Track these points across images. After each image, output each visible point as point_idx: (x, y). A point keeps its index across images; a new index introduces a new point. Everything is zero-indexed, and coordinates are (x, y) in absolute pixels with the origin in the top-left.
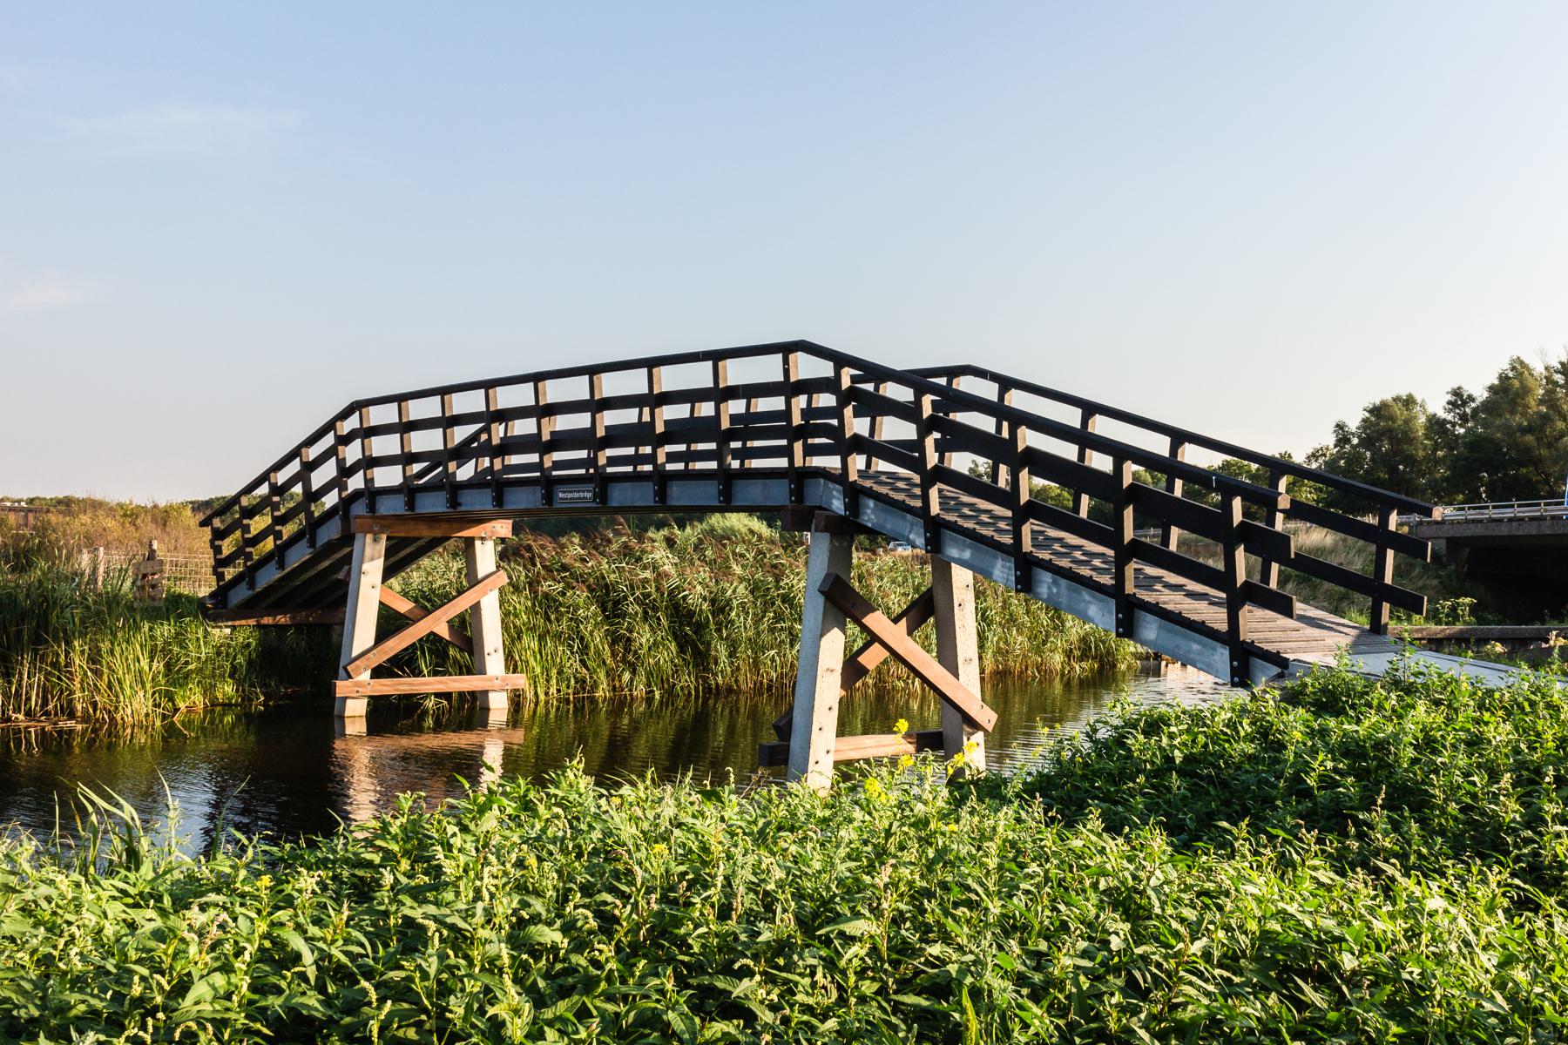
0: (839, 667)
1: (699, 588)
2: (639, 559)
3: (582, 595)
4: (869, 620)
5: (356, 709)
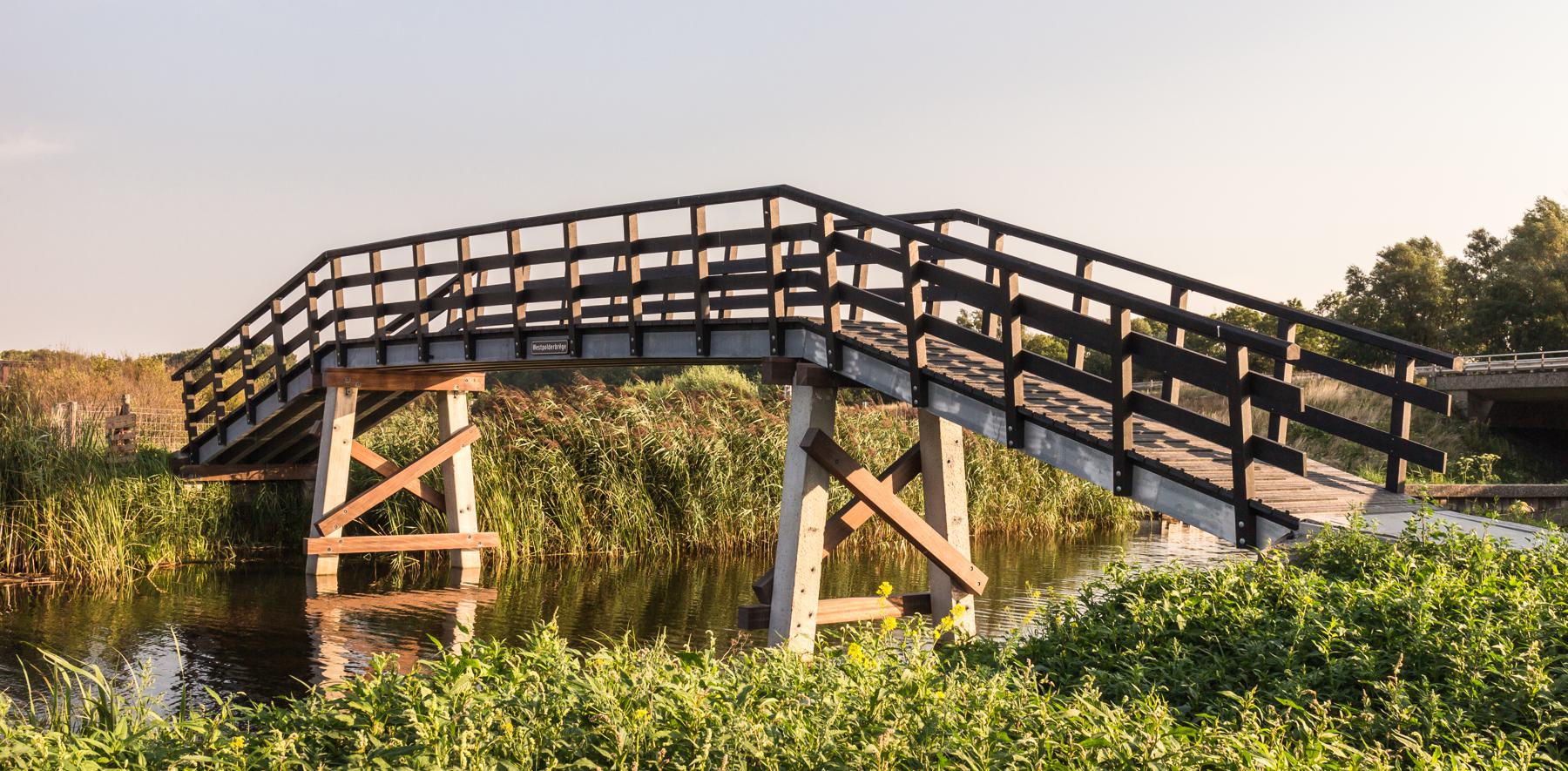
3: (552, 452)
4: (853, 478)
5: (328, 567)
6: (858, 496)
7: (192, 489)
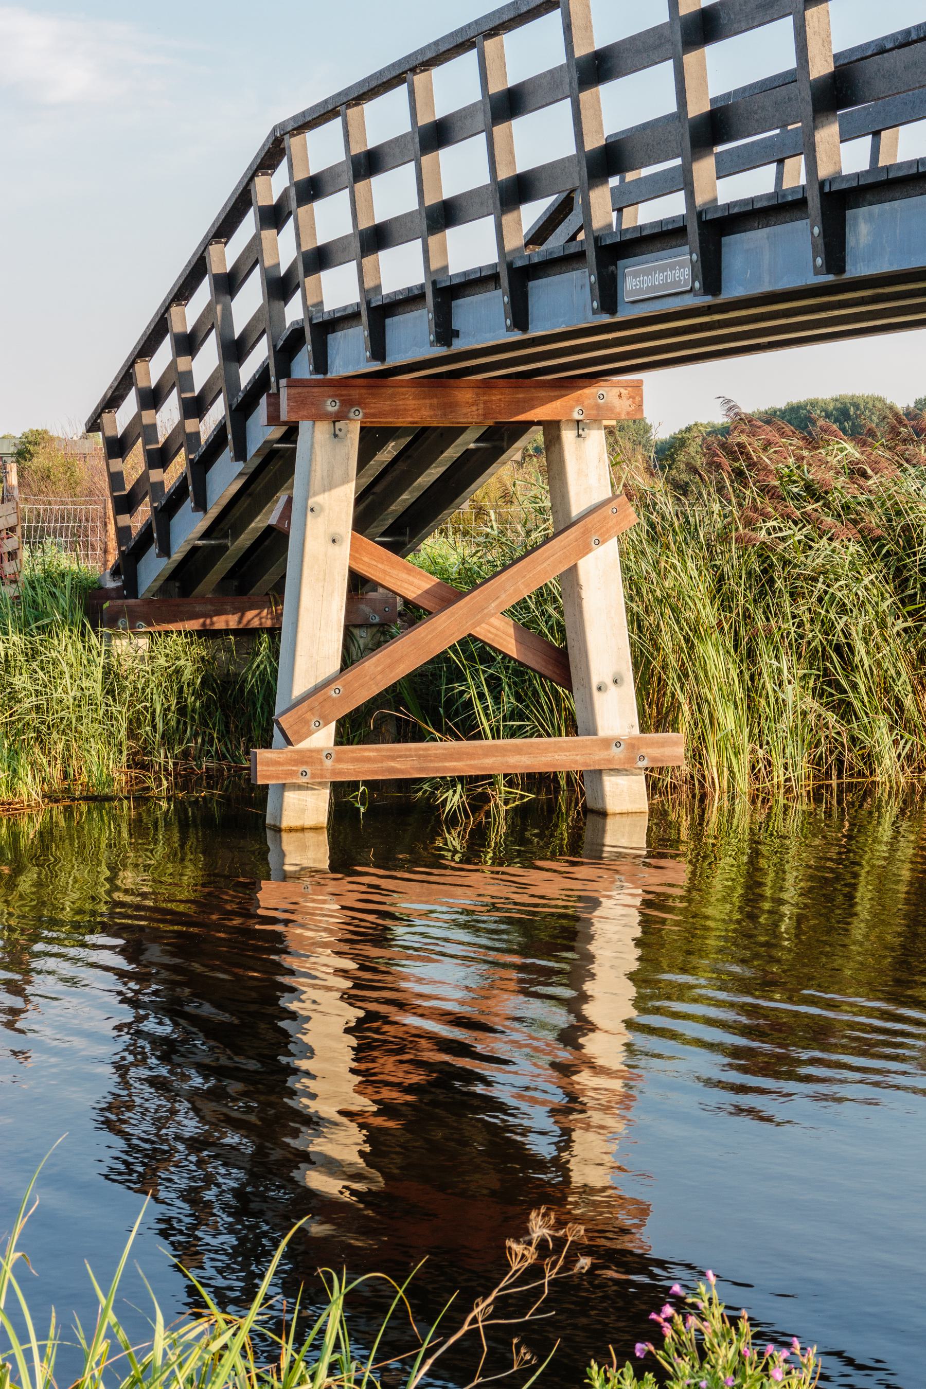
5: (304, 809)
7: (131, 648)
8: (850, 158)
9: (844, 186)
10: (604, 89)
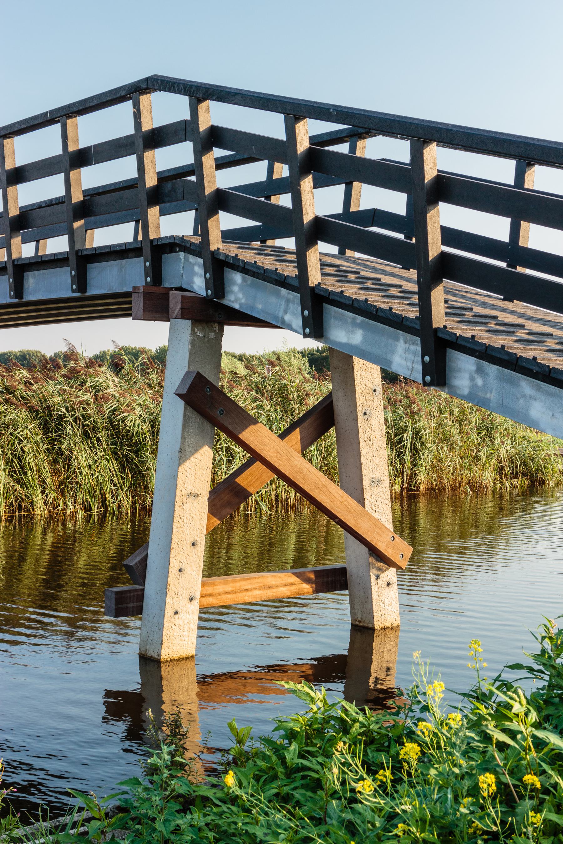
0: (205, 489)
1: (138, 409)
2: (83, 383)
4: (247, 435)
6: (256, 457)
8: (27, 251)
9: (23, 262)
10: (20, 187)
